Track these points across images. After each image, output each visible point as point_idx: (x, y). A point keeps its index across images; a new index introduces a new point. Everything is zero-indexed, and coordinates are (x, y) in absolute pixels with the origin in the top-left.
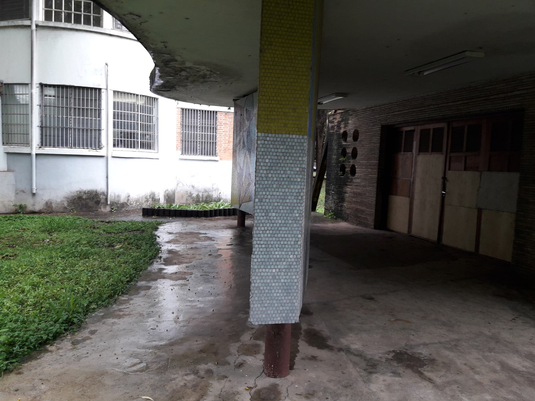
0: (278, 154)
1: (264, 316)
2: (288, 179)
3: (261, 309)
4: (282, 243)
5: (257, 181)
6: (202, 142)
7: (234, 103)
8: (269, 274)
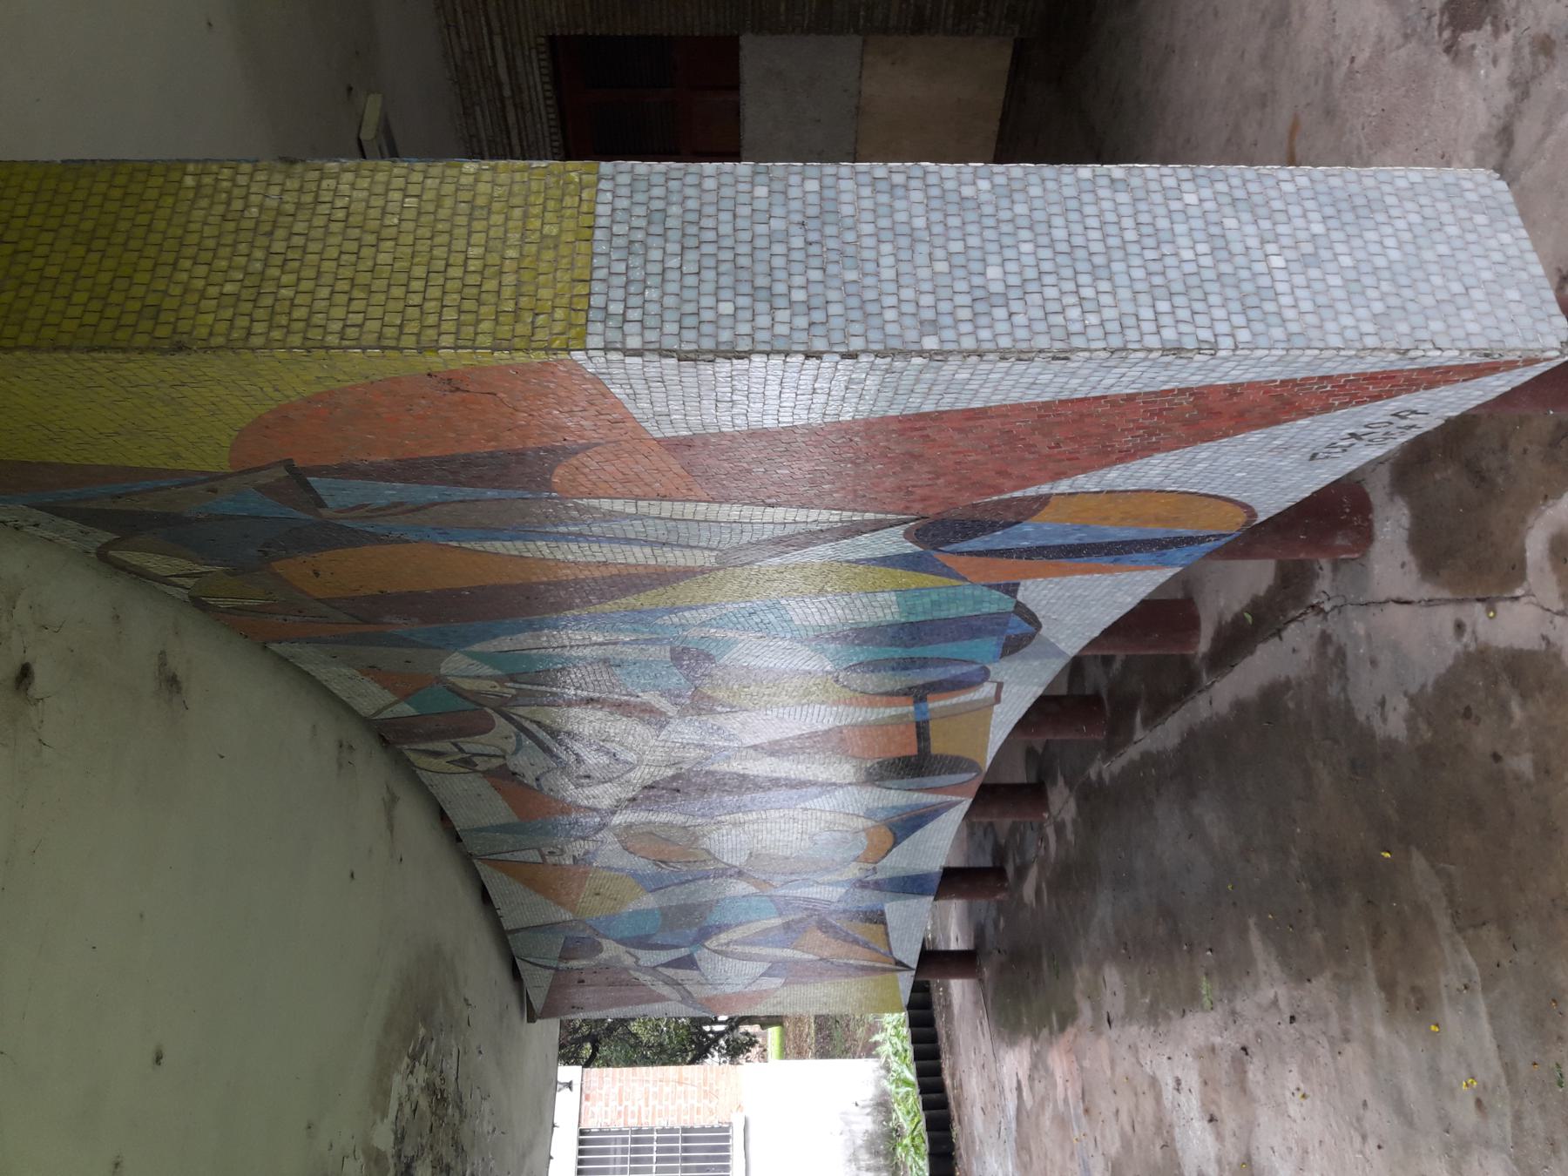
0: (690, 268)
2: (812, 224)
3: (1483, 307)
4: (1130, 235)
5: (831, 344)
7: (540, 1018)
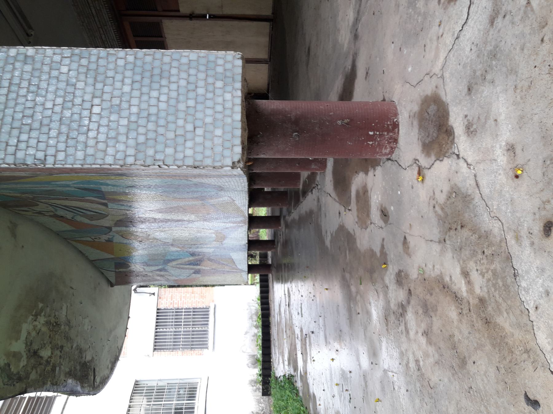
1: (219, 132)
3: (199, 140)
6: (193, 325)
8: (104, 122)
